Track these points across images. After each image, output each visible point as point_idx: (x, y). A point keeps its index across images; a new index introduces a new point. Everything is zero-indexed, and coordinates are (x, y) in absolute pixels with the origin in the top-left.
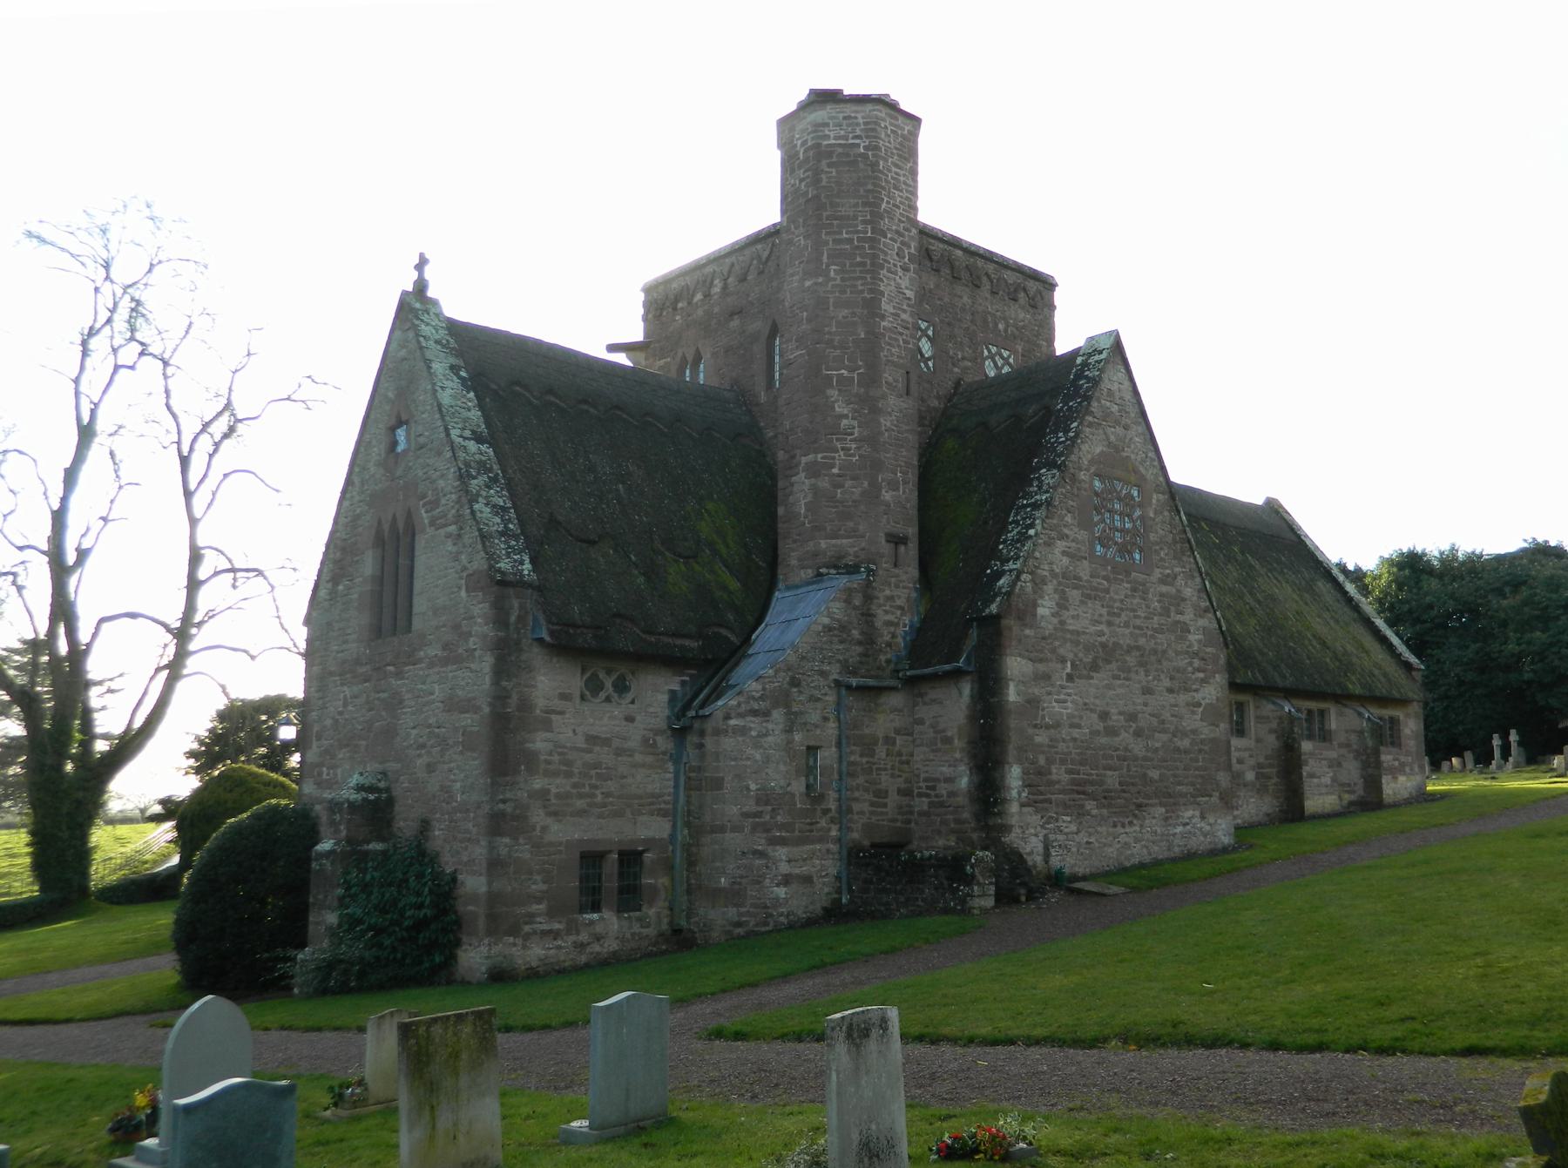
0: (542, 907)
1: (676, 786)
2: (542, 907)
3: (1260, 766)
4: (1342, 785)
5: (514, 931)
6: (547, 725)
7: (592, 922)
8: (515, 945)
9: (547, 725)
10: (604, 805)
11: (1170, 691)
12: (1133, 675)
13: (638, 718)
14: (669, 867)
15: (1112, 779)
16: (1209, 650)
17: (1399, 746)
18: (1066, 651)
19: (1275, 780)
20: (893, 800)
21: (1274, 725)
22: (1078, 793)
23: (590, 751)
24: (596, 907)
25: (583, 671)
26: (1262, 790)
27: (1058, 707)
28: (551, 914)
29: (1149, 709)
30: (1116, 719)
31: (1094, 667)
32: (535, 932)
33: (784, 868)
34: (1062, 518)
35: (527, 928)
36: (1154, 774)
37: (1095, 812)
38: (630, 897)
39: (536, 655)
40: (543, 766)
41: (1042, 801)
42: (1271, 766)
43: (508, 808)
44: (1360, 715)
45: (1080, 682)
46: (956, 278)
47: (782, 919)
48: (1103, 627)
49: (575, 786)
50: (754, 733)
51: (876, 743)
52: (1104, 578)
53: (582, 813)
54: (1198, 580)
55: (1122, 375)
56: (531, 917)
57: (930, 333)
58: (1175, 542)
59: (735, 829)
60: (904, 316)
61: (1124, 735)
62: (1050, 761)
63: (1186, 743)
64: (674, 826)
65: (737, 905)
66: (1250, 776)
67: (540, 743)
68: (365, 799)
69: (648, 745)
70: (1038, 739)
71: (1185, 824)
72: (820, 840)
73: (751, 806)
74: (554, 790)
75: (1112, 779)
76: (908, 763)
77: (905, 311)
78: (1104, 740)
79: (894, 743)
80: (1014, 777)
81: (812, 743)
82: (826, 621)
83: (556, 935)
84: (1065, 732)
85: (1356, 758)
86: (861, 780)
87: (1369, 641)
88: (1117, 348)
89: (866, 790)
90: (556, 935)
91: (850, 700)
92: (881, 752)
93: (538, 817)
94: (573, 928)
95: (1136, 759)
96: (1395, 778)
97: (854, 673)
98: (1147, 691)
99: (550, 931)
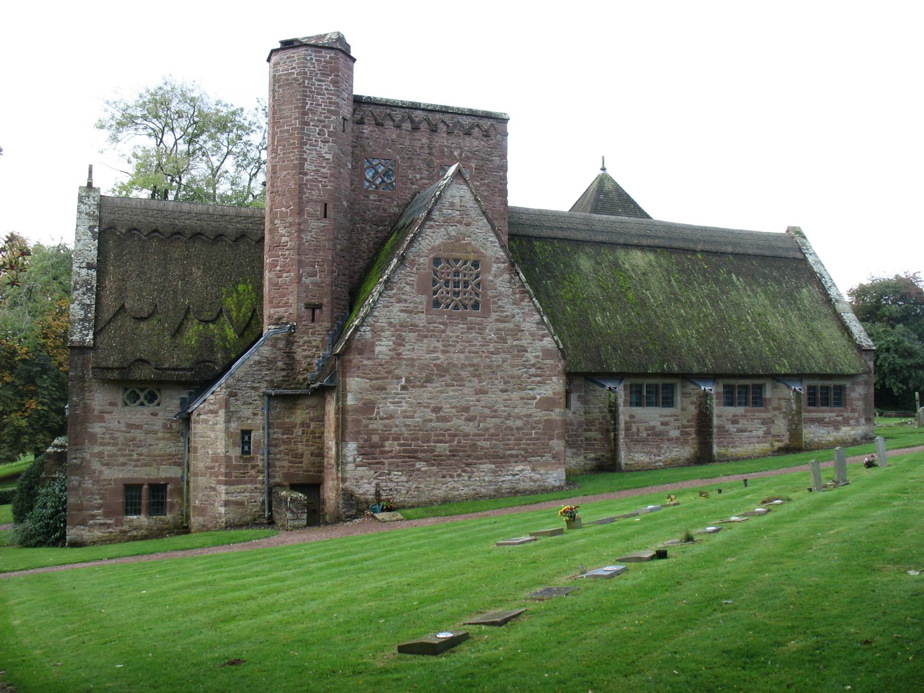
5: (83, 523)
6: (101, 419)
7: (131, 521)
10: (138, 460)
13: (160, 414)
19: (694, 436)
20: (307, 460)
22: (409, 457)
24: (138, 512)
28: (107, 515)
29: (483, 403)
30: (447, 410)
31: (429, 380)
32: (96, 524)
35: (91, 522)
39: (95, 385)
40: (100, 440)
41: (376, 463)
42: (691, 426)
45: (416, 391)
49: (120, 450)
53: (124, 464)
56: (93, 517)
58: (514, 293)
59: (203, 475)
60: (323, 170)
63: (519, 423)
65: (204, 516)
66: (674, 433)
68: (55, 452)
71: (514, 475)
72: (251, 482)
73: (209, 463)
74: (106, 453)
75: (442, 448)
76: (320, 437)
77: (324, 167)
79: (309, 426)
81: (245, 428)
83: (109, 526)
85: (784, 417)
86: (282, 448)
89: (287, 454)
90: (109, 526)
92: (298, 431)
93: (96, 465)
95: (466, 435)
97: (278, 387)
99: (105, 524)
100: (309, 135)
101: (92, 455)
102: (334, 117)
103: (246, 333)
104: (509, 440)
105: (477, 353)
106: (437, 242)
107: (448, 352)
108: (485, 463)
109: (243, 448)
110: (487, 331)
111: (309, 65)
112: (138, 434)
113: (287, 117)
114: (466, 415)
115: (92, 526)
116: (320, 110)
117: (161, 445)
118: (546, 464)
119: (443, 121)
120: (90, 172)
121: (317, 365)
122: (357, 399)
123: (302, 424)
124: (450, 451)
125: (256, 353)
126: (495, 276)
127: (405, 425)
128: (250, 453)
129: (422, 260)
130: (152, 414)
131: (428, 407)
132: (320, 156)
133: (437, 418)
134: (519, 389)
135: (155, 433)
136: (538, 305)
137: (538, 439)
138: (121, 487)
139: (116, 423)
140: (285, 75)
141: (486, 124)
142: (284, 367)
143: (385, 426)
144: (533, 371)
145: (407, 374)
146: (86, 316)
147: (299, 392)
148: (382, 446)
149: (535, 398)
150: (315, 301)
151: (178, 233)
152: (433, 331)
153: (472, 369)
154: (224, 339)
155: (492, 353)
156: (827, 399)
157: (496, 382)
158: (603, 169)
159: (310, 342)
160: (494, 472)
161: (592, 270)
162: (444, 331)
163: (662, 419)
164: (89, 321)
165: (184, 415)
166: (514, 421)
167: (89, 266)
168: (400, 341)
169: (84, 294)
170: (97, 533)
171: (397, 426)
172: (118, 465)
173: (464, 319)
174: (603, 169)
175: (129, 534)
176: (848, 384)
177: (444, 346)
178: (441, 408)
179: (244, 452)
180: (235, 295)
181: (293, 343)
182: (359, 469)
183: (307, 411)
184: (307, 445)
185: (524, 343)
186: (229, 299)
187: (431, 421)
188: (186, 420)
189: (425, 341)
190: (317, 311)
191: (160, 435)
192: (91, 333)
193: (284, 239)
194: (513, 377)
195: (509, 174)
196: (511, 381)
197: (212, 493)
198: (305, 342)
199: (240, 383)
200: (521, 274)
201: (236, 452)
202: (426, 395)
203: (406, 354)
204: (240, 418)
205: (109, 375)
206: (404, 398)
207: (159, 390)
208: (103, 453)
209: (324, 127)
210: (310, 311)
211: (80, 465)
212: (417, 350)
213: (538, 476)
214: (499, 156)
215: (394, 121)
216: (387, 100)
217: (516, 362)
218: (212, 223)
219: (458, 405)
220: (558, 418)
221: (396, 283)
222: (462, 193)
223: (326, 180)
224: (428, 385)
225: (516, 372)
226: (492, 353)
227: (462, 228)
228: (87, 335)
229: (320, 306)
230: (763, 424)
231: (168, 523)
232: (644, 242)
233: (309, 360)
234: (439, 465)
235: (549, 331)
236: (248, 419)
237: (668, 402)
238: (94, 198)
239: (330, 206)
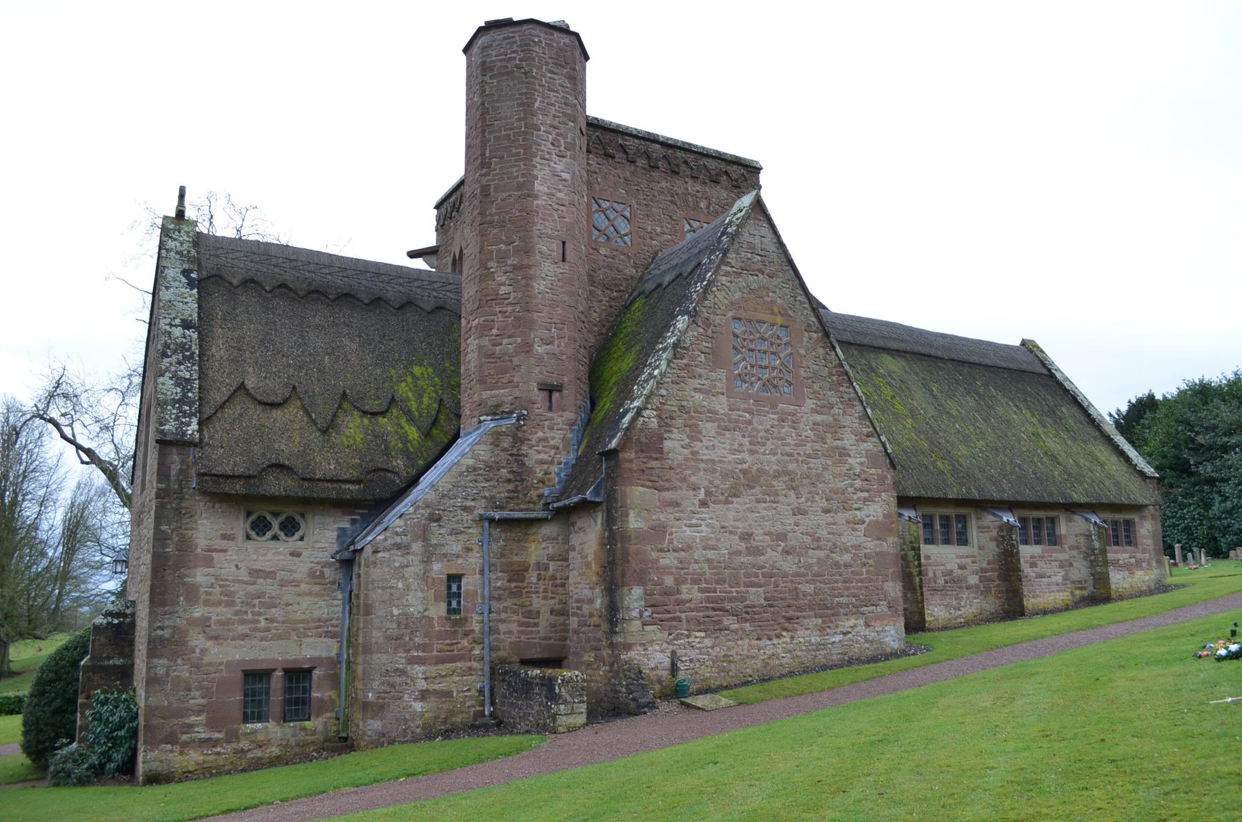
0: (202, 718)
1: (343, 612)
2: (202, 718)
3: (984, 570)
4: (1073, 582)
5: (172, 739)
6: (209, 562)
7: (254, 732)
8: (171, 751)
9: (209, 562)
10: (268, 630)
11: (827, 511)
12: (781, 498)
13: (305, 553)
14: (334, 681)
15: (756, 596)
16: (873, 471)
17: (1136, 545)
18: (701, 479)
20: (545, 620)
21: (994, 534)
22: (714, 609)
23: (254, 584)
24: (260, 718)
25: (249, 514)
26: (986, 592)
27: (682, 532)
29: (802, 528)
30: (760, 538)
33: (422, 685)
34: (693, 358)
35: (185, 737)
36: (809, 589)
37: (733, 627)
38: (297, 705)
39: (199, 505)
40: (203, 597)
42: (992, 570)
43: (166, 633)
44: (1087, 520)
46: (655, 167)
47: (418, 730)
48: (746, 456)
49: (236, 613)
50: (397, 564)
51: (526, 570)
52: (745, 411)
53: (244, 637)
54: (859, 408)
55: (766, 231)
56: (189, 727)
57: (627, 214)
60: (560, 195)
61: (770, 552)
62: (679, 581)
63: (847, 557)
64: (341, 648)
66: (973, 580)
67: (200, 577)
68: (108, 623)
69: (315, 576)
70: (663, 562)
75: (756, 596)
76: (563, 585)
77: (560, 191)
78: (746, 559)
79: (547, 569)
80: (634, 598)
81: (453, 571)
82: (471, 462)
84: (697, 554)
87: (1104, 453)
89: (515, 612)
91: (496, 532)
93: (197, 641)
94: (232, 737)
95: (785, 575)
96: (1132, 573)
97: (501, 508)
98: (798, 512)
101: (192, 622)
103: (434, 432)
104: (836, 582)
108: (810, 617)
109: (449, 604)
110: (801, 425)
112: (264, 585)
113: (506, 118)
114: (783, 544)
115: (185, 745)
117: (304, 605)
118: (880, 618)
119: (685, 162)
120: (182, 196)
121: (558, 474)
123: (538, 565)
124: (766, 599)
127: (709, 561)
128: (459, 610)
130: (292, 554)
135: (296, 583)
137: (871, 581)
138: (239, 676)
139: (234, 569)
140: (501, 61)
142: (511, 476)
143: (681, 562)
144: (858, 483)
145: (706, 483)
146: (184, 395)
147: (533, 515)
148: (679, 592)
149: (863, 522)
151: (317, 292)
153: (786, 479)
154: (404, 439)
155: (809, 456)
156: (1117, 537)
159: (545, 439)
160: (822, 630)
163: (959, 561)
164: (190, 404)
165: (346, 555)
167: (186, 325)
169: (180, 363)
170: (194, 757)
171: (696, 562)
172: (233, 639)
175: (250, 755)
176: (1136, 518)
179: (451, 611)
180: (409, 379)
182: (647, 628)
183: (544, 545)
184: (545, 598)
185: (846, 443)
186: (403, 385)
187: (739, 553)
188: (348, 562)
189: (728, 434)
190: (556, 395)
191: (304, 587)
192: (195, 421)
193: (503, 290)
194: (836, 493)
197: (398, 680)
198: (541, 440)
199: (445, 500)
200: (838, 349)
201: (438, 610)
202: (731, 514)
204: (445, 555)
205: (227, 488)
207: (303, 516)
208: (209, 618)
210: (546, 394)
211: (168, 640)
213: (874, 634)
215: (627, 153)
216: (619, 125)
218: (364, 282)
219: (773, 530)
220: (891, 551)
224: (734, 499)
226: (809, 456)
228: (189, 425)
229: (559, 388)
230: (1061, 567)
231: (314, 733)
232: (895, 345)
234: (752, 620)
237: (963, 541)
238: (187, 233)
239: (569, 246)
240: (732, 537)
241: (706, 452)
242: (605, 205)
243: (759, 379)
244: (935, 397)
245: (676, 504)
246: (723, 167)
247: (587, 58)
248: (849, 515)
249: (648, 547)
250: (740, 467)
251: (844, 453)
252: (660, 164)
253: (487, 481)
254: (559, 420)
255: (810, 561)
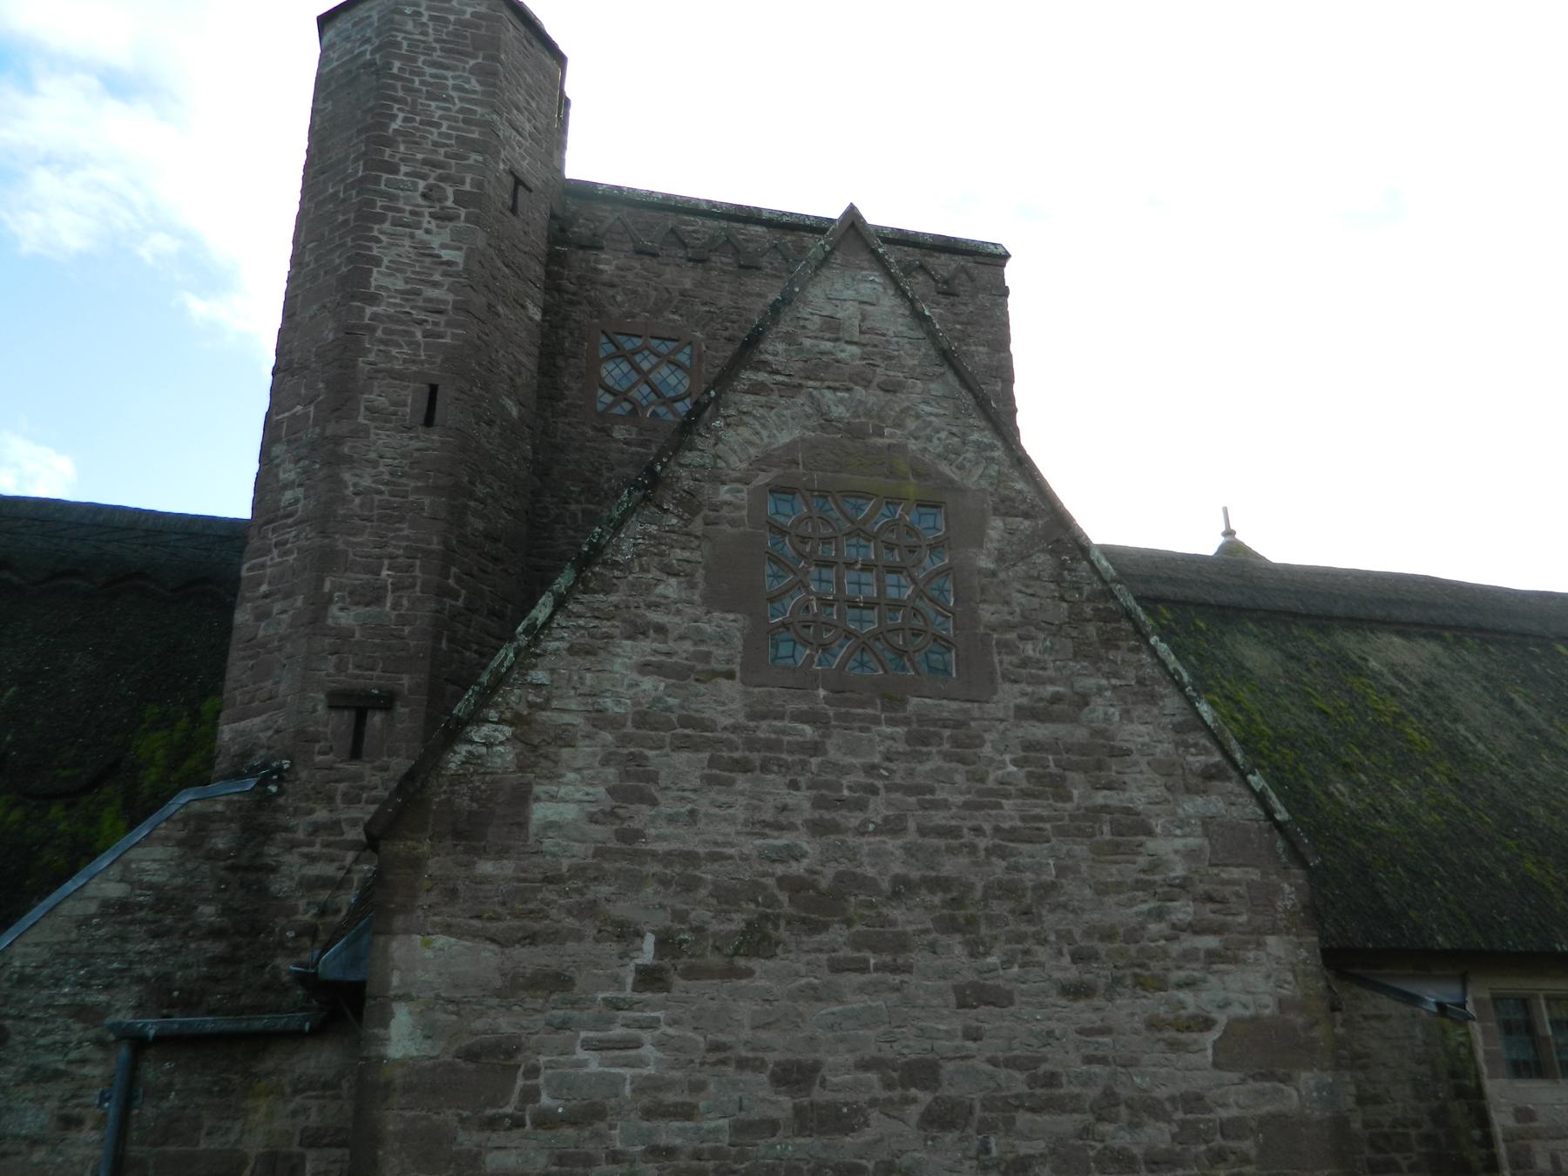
12: (918, 958)
16: (1235, 873)
18: (647, 908)
30: (842, 1080)
31: (757, 941)
48: (804, 842)
52: (799, 717)
54: (1173, 703)
57: (683, 358)
58: (1076, 618)
63: (1158, 1135)
77: (435, 284)
88: (991, 259)
97: (189, 1003)
98: (973, 996)
100: (392, 198)
102: (475, 157)
105: (954, 832)
106: (784, 438)
107: (835, 828)
111: (410, 26)
114: (925, 1097)
116: (435, 137)
122: (430, 1032)
125: (116, 871)
126: (1001, 557)
129: (724, 493)
131: (759, 1066)
132: (424, 251)
133: (798, 1111)
134: (1139, 982)
136: (1172, 661)
141: (944, 265)
144: (1183, 910)
145: (663, 919)
147: (282, 1022)
150: (374, 680)
152: (771, 745)
153: (937, 899)
157: (1042, 953)
158: (1229, 533)
159: (334, 826)
161: (1280, 671)
162: (816, 748)
166: (1134, 1126)
168: (636, 784)
173: (893, 702)
174: (1229, 533)
177: (818, 803)
178: (816, 1067)
181: (268, 833)
189: (742, 782)
190: (376, 719)
194: (1108, 935)
195: (1018, 390)
196: (1102, 948)
198: (317, 828)
203: (662, 836)
206: (652, 1024)
209: (441, 178)
210: (348, 716)
212: (718, 824)
214: (988, 344)
217: (1113, 873)
219: (888, 1053)
221: (626, 567)
222: (866, 289)
223: (442, 319)
224: (755, 964)
225: (1121, 913)
226: (1012, 835)
227: (870, 397)
229: (386, 702)
233: (323, 895)
235: (1227, 755)
236: (34, 1142)
240: (748, 1076)
241: (668, 830)
242: (629, 344)
243: (849, 634)
244: (1519, 714)
245: (557, 982)
246: (914, 256)
247: (561, 59)
248: (1155, 1004)
249: (449, 1115)
250: (780, 869)
251: (1133, 826)
252: (764, 262)
253: (155, 935)
254: (376, 779)
255: (1024, 1148)
